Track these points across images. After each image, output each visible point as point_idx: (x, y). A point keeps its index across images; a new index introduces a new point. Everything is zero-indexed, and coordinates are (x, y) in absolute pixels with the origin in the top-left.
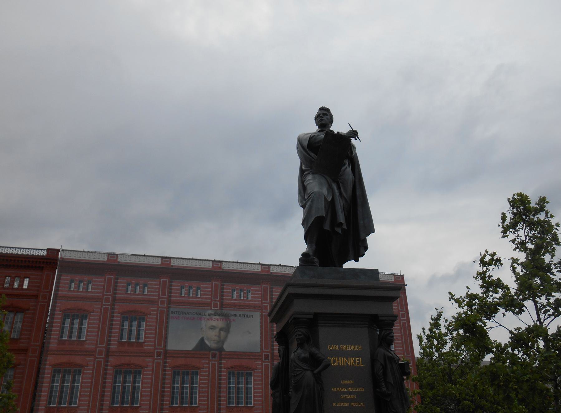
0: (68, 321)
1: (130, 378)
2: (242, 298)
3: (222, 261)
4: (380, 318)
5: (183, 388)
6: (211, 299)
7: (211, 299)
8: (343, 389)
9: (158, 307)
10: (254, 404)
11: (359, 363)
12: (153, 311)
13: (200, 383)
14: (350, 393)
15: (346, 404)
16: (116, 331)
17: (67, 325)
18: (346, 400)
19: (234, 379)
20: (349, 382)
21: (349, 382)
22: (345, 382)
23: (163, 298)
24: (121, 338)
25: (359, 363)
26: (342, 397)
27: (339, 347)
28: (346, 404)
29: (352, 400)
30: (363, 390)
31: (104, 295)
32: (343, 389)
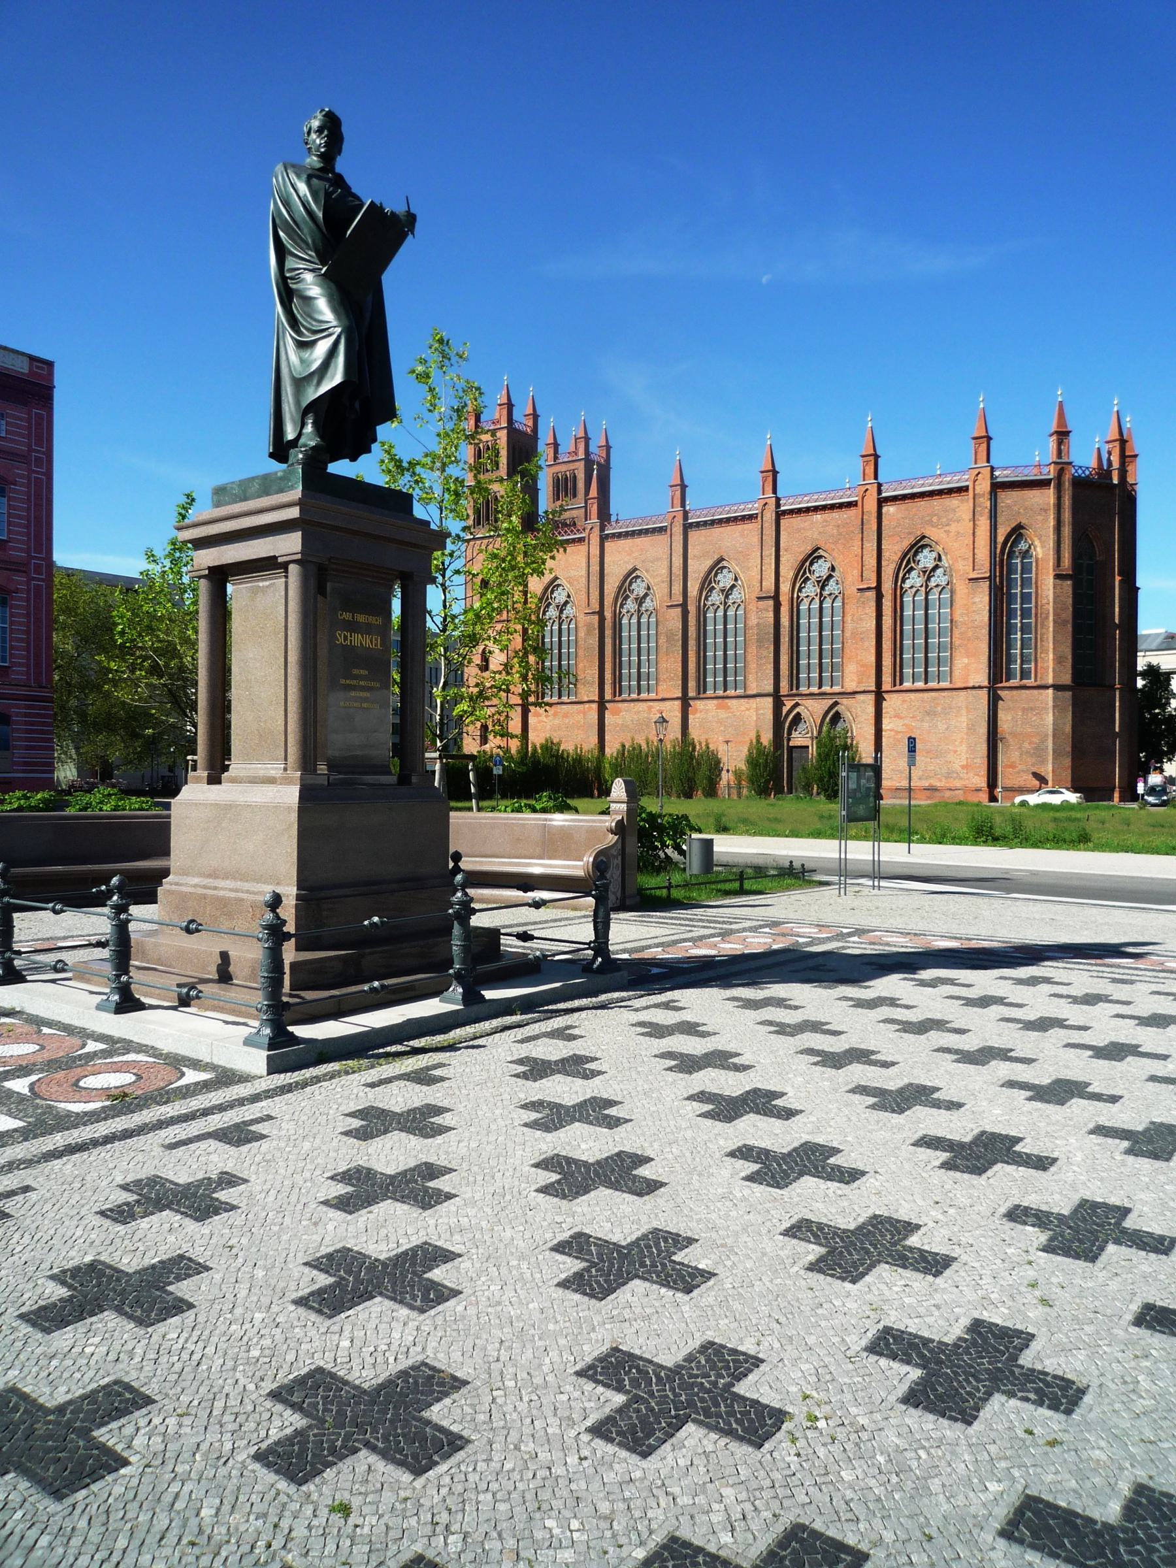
9: (30, 471)
12: (22, 476)
21: (364, 672)
31: (30, 450)
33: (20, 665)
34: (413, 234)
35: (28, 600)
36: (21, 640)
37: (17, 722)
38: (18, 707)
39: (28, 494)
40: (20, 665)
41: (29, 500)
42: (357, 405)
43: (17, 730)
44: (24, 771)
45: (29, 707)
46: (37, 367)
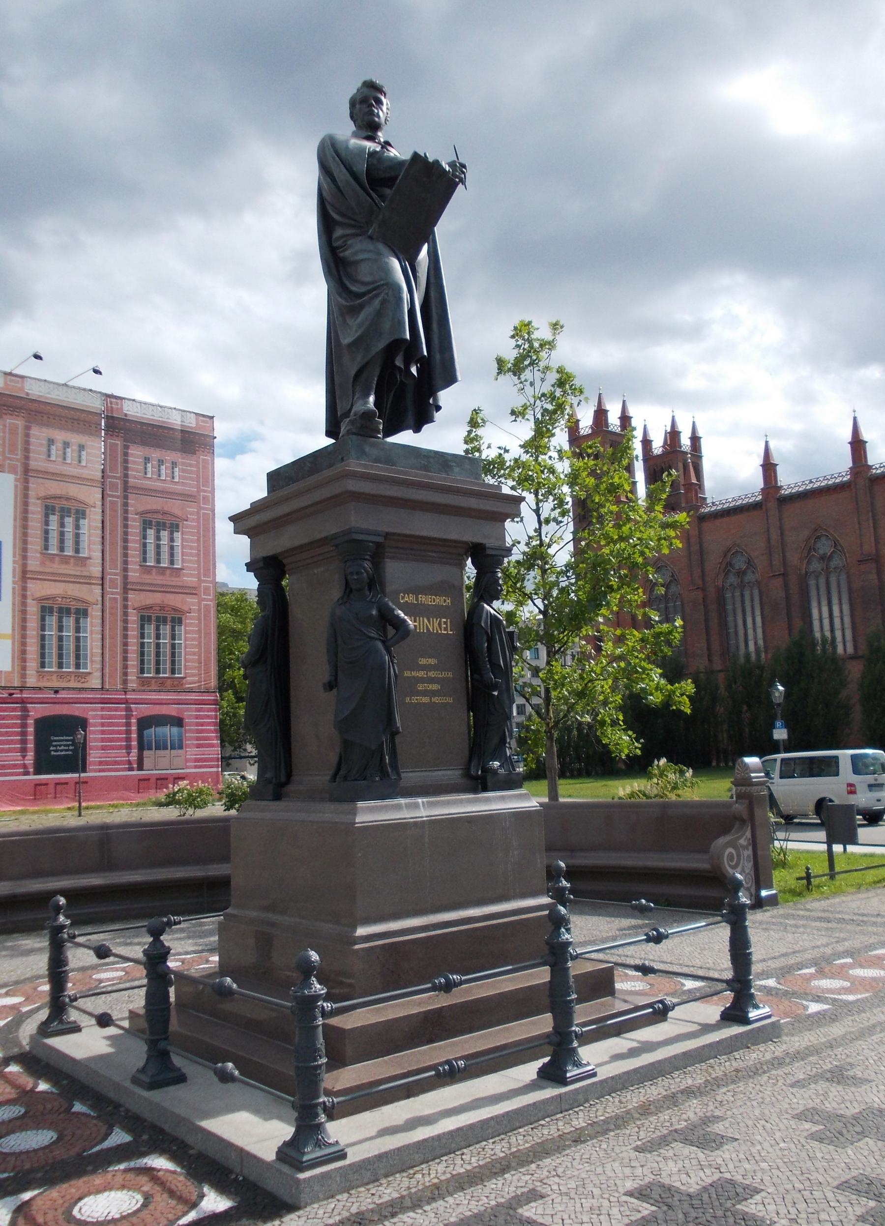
0: (151, 533)
1: (166, 630)
2: (149, 475)
3: (125, 399)
4: (489, 552)
5: (158, 646)
6: (198, 487)
8: (421, 674)
10: (186, 673)
11: (446, 629)
13: (91, 631)
14: (432, 681)
15: (425, 700)
16: (134, 546)
17: (151, 540)
18: (425, 693)
19: (52, 621)
20: (432, 661)
21: (432, 661)
22: (423, 661)
24: (145, 560)
25: (446, 629)
26: (420, 687)
27: (417, 599)
28: (425, 700)
29: (433, 693)
30: (450, 675)
32: (421, 674)
33: (193, 675)
34: (464, 183)
35: (199, 619)
36: (194, 654)
37: (190, 724)
38: (95, 710)
39: (198, 527)
40: (193, 675)
41: (199, 533)
42: (414, 370)
43: (191, 731)
44: (196, 767)
45: (102, 709)
46: (203, 421)
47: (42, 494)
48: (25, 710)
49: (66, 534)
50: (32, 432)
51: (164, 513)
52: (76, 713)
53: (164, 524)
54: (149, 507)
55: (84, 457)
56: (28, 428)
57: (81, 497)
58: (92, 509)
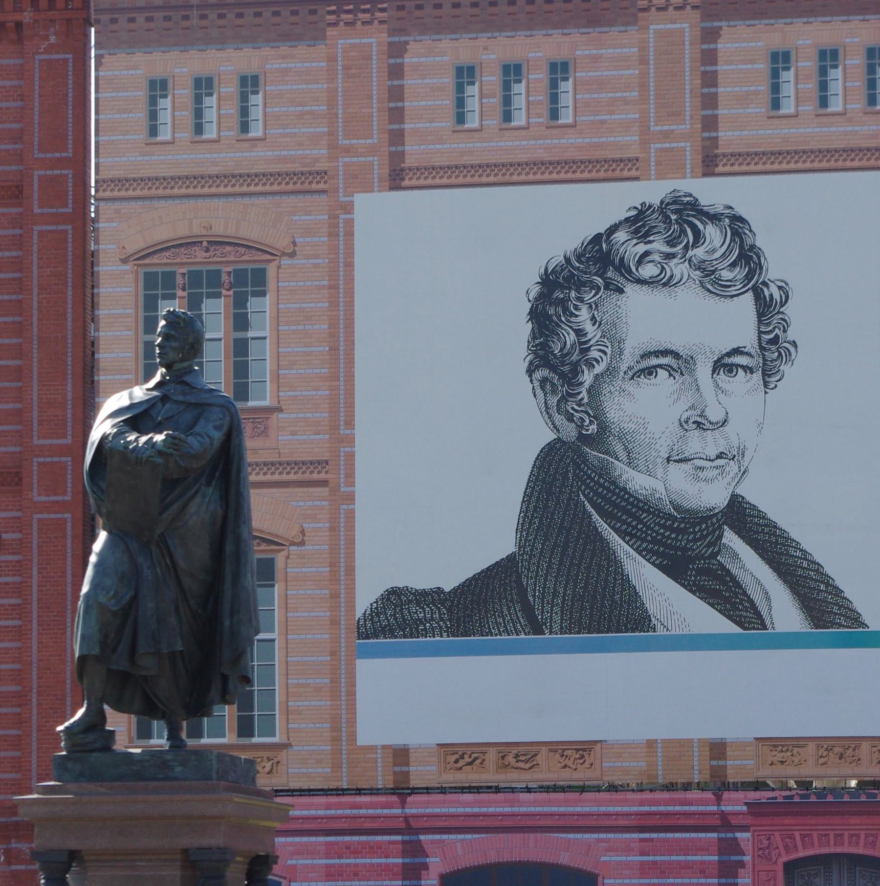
7: (333, 146)
23: (666, 135)
38: (311, 852)
47: (136, 244)
48: (414, 849)
49: (252, 346)
50: (722, 45)
51: (216, 244)
52: (564, 859)
53: (214, 279)
54: (162, 234)
55: (256, 113)
56: (397, 50)
57: (251, 232)
58: (286, 261)
